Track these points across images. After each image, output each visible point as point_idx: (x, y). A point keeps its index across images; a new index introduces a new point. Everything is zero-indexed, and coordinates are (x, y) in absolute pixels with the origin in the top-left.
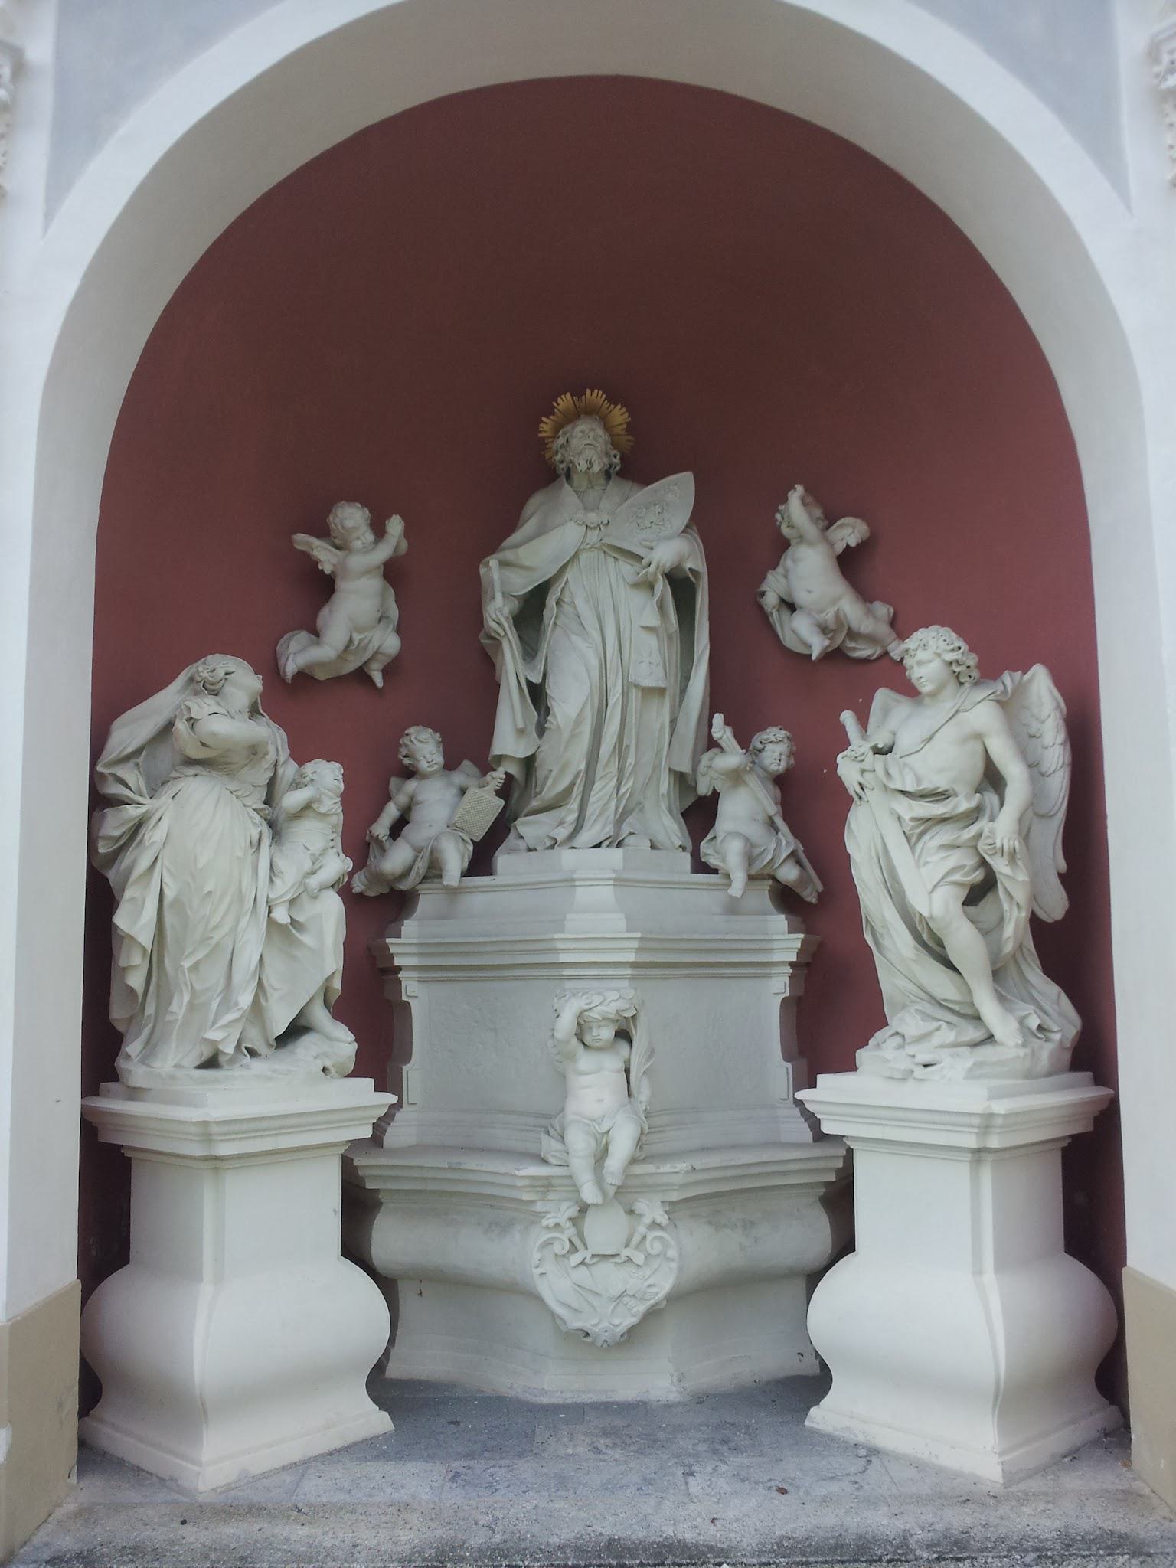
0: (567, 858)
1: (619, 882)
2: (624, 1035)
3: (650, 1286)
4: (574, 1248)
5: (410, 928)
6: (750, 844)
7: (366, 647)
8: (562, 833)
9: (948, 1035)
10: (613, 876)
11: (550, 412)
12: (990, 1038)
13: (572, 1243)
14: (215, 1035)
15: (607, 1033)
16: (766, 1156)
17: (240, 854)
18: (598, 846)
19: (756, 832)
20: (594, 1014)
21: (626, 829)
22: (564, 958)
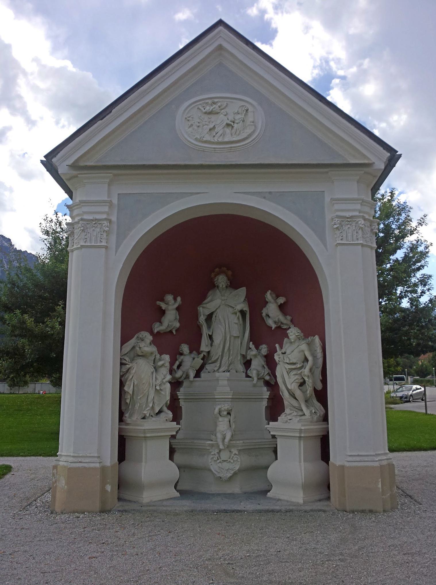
0: (217, 374)
1: (228, 380)
2: (229, 414)
3: (234, 467)
4: (218, 459)
5: (182, 389)
6: (258, 371)
7: (172, 326)
8: (216, 369)
9: (295, 414)
10: (227, 379)
11: (214, 272)
12: (304, 415)
13: (218, 458)
14: (145, 412)
15: (225, 413)
16: (260, 441)
17: (149, 375)
18: (224, 372)
19: (260, 369)
20: (223, 409)
21: (230, 368)
22: (216, 397)
